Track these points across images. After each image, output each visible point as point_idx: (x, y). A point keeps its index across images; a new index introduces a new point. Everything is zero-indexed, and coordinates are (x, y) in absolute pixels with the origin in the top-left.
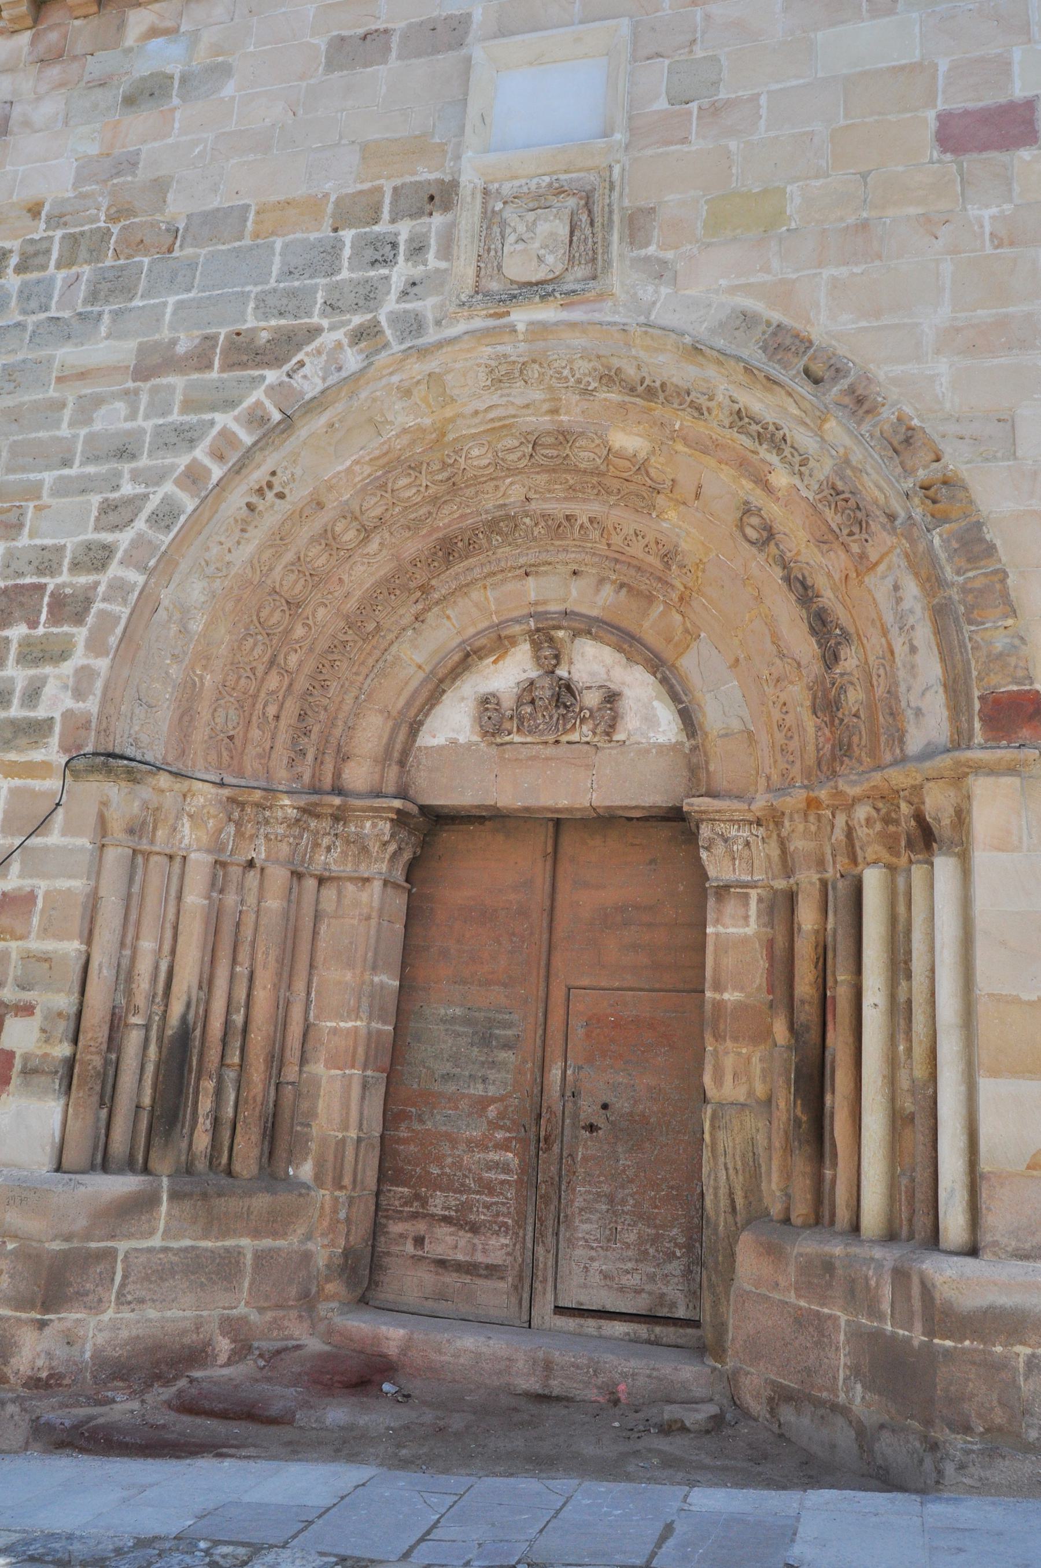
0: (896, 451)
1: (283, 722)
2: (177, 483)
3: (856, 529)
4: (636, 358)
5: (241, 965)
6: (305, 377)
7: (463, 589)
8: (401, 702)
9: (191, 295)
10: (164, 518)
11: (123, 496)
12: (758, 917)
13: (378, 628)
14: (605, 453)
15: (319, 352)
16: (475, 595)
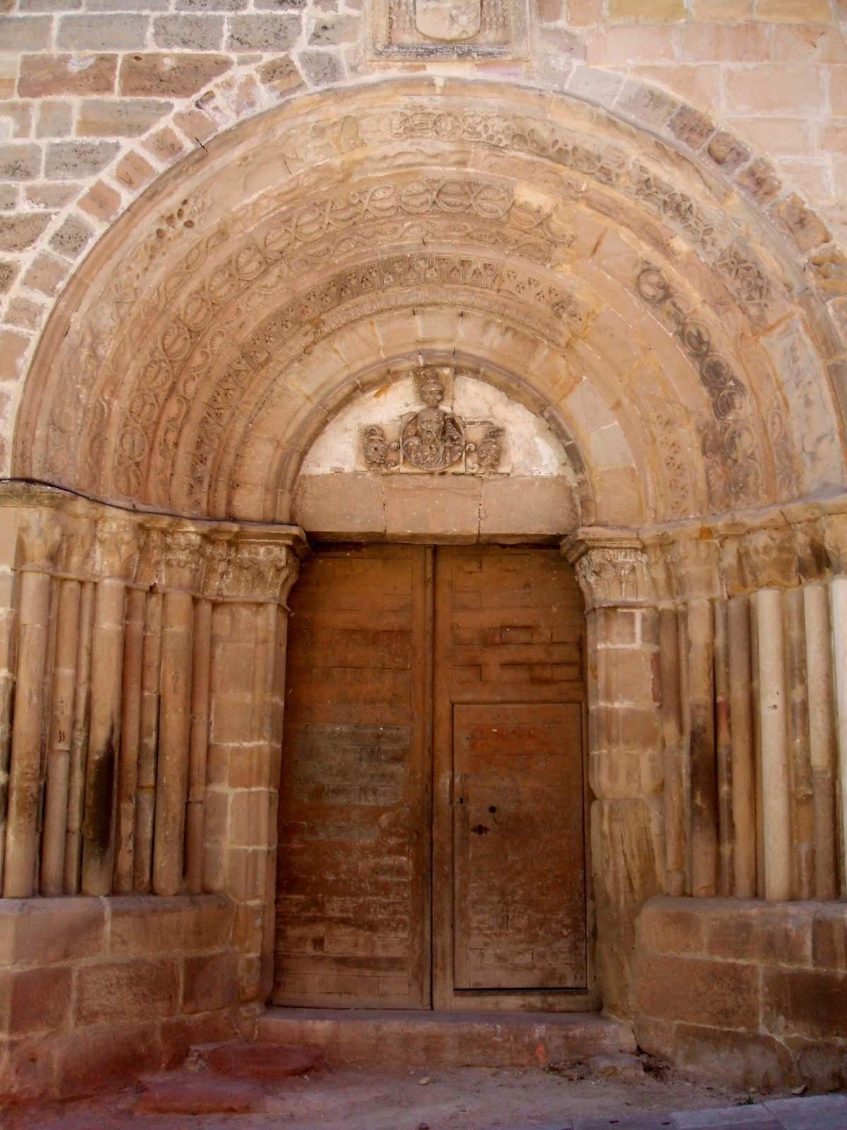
0: (791, 230)
1: (182, 451)
2: (81, 204)
3: (756, 295)
4: (551, 122)
5: (149, 690)
6: (216, 109)
7: (351, 324)
8: (290, 432)
9: (80, 12)
10: (70, 238)
11: (19, 215)
12: (643, 634)
13: (268, 360)
14: (509, 206)
15: (229, 85)
16: (363, 329)
